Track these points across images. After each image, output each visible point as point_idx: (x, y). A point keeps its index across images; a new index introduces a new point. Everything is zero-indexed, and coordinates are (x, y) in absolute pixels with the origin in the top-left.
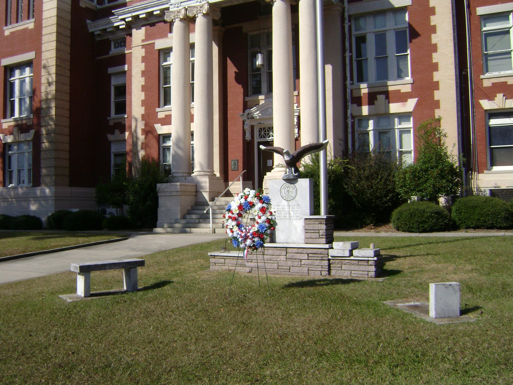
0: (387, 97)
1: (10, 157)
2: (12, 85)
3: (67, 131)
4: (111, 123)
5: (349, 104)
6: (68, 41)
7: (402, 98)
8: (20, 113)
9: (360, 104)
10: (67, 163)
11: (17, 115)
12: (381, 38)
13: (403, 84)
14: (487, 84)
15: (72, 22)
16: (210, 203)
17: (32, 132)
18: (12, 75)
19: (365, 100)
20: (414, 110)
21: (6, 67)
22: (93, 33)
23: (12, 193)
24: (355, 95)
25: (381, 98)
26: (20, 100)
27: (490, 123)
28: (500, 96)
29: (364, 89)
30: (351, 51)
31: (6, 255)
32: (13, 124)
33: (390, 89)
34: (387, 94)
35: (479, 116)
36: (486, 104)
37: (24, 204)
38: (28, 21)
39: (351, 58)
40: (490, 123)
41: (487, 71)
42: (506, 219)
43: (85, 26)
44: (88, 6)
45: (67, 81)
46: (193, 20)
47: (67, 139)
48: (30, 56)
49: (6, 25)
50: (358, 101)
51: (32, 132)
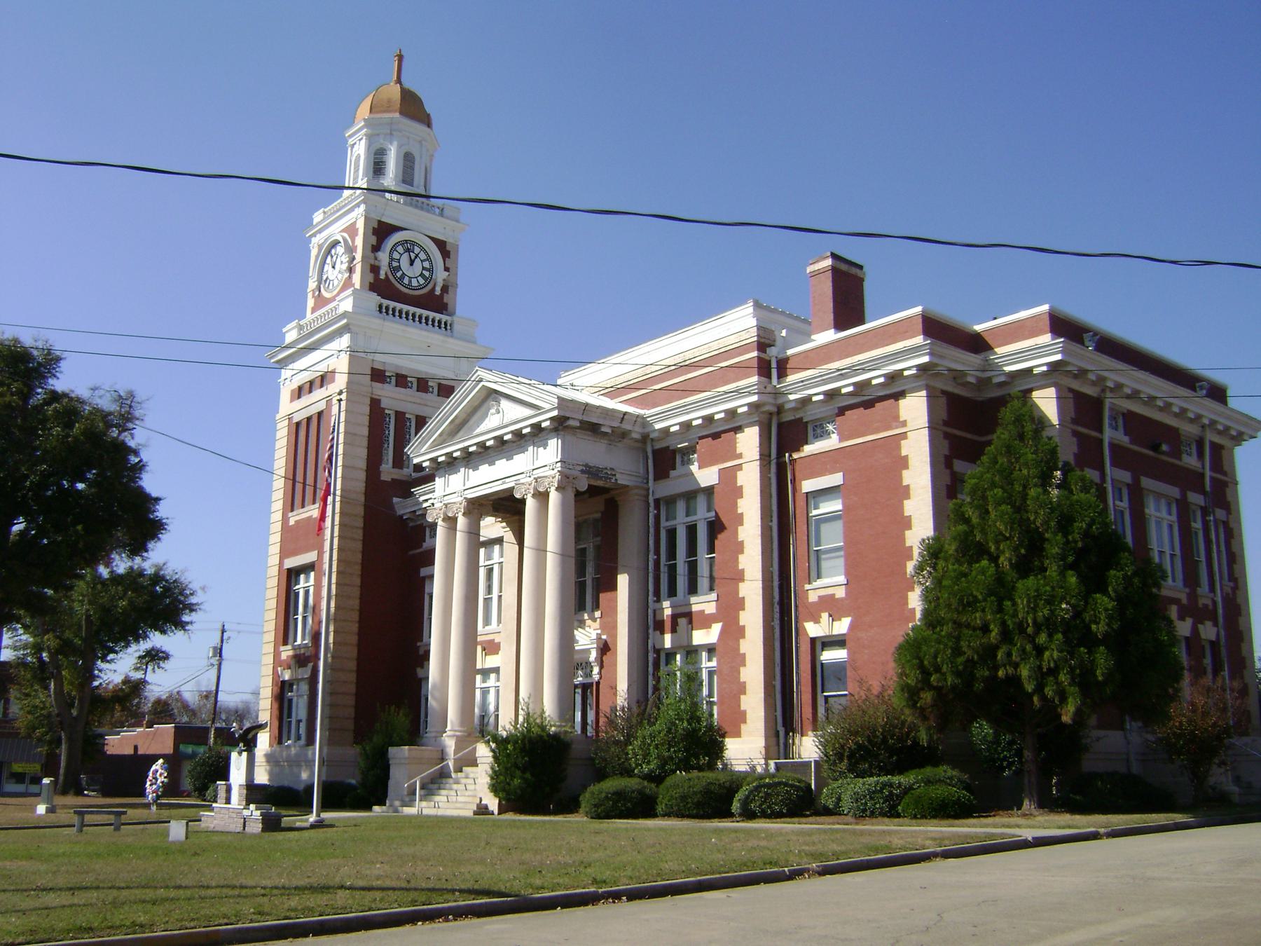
0: (690, 622)
1: (290, 701)
2: (297, 595)
3: (353, 665)
5: (651, 631)
6: (359, 534)
7: (707, 621)
8: (303, 639)
9: (663, 633)
10: (351, 712)
11: (299, 642)
12: (692, 530)
13: (704, 603)
14: (813, 597)
15: (366, 507)
16: (453, 775)
17: (311, 665)
18: (297, 583)
19: (668, 625)
20: (719, 639)
21: (289, 570)
22: (401, 517)
23: (284, 754)
24: (658, 618)
25: (682, 622)
26: (305, 618)
27: (822, 658)
29: (667, 609)
30: (657, 552)
31: (615, 884)
32: (291, 653)
33: (695, 608)
34: (689, 615)
35: (805, 648)
36: (813, 630)
37: (295, 770)
38: (313, 507)
39: (657, 563)
40: (822, 658)
41: (819, 577)
42: (698, 805)
43: (391, 507)
44: (395, 477)
45: (356, 592)
46: (455, 519)
47: (352, 677)
48: (311, 557)
49: (292, 510)
50: (659, 626)
51: (311, 665)
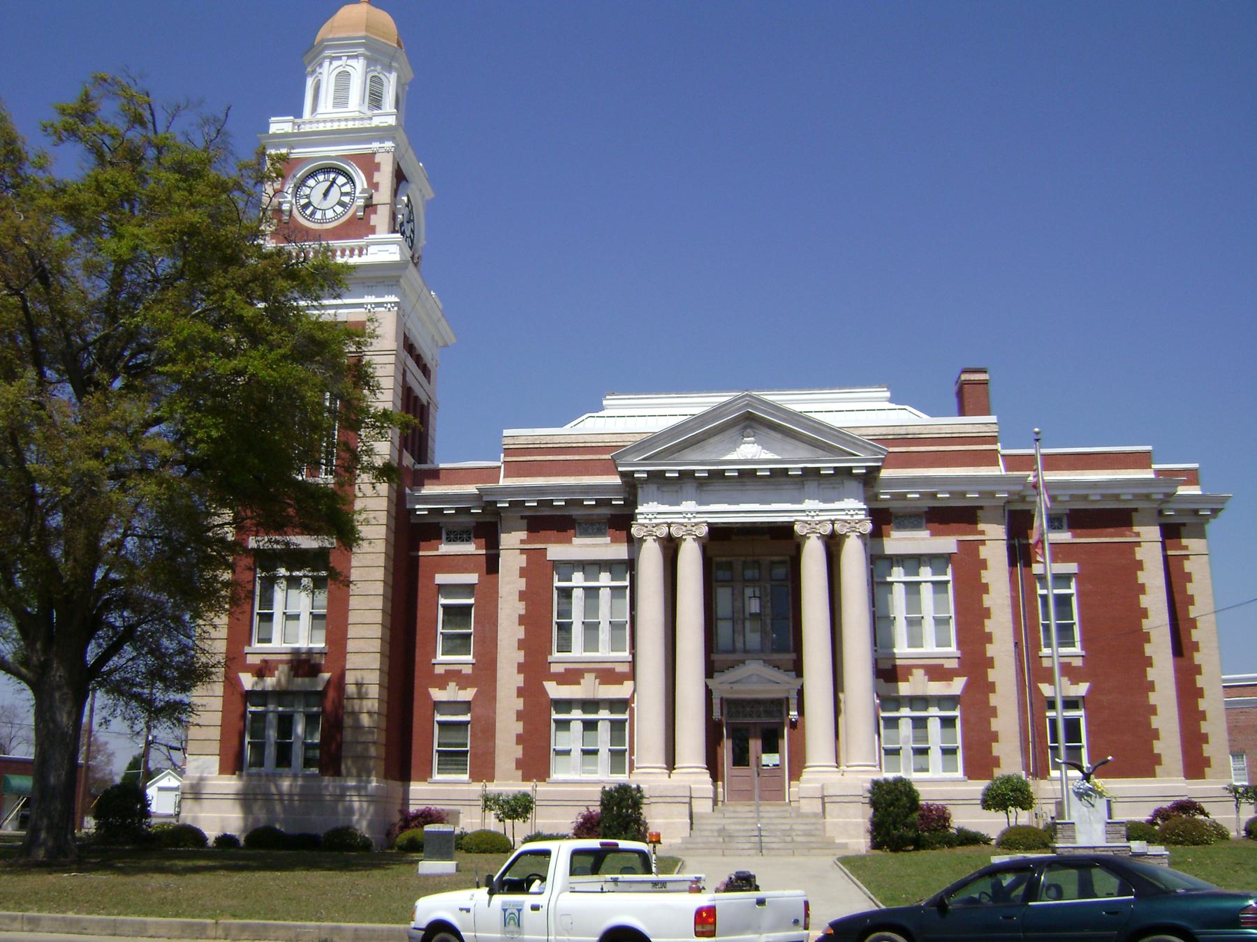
4: (439, 670)
28: (452, 685)
